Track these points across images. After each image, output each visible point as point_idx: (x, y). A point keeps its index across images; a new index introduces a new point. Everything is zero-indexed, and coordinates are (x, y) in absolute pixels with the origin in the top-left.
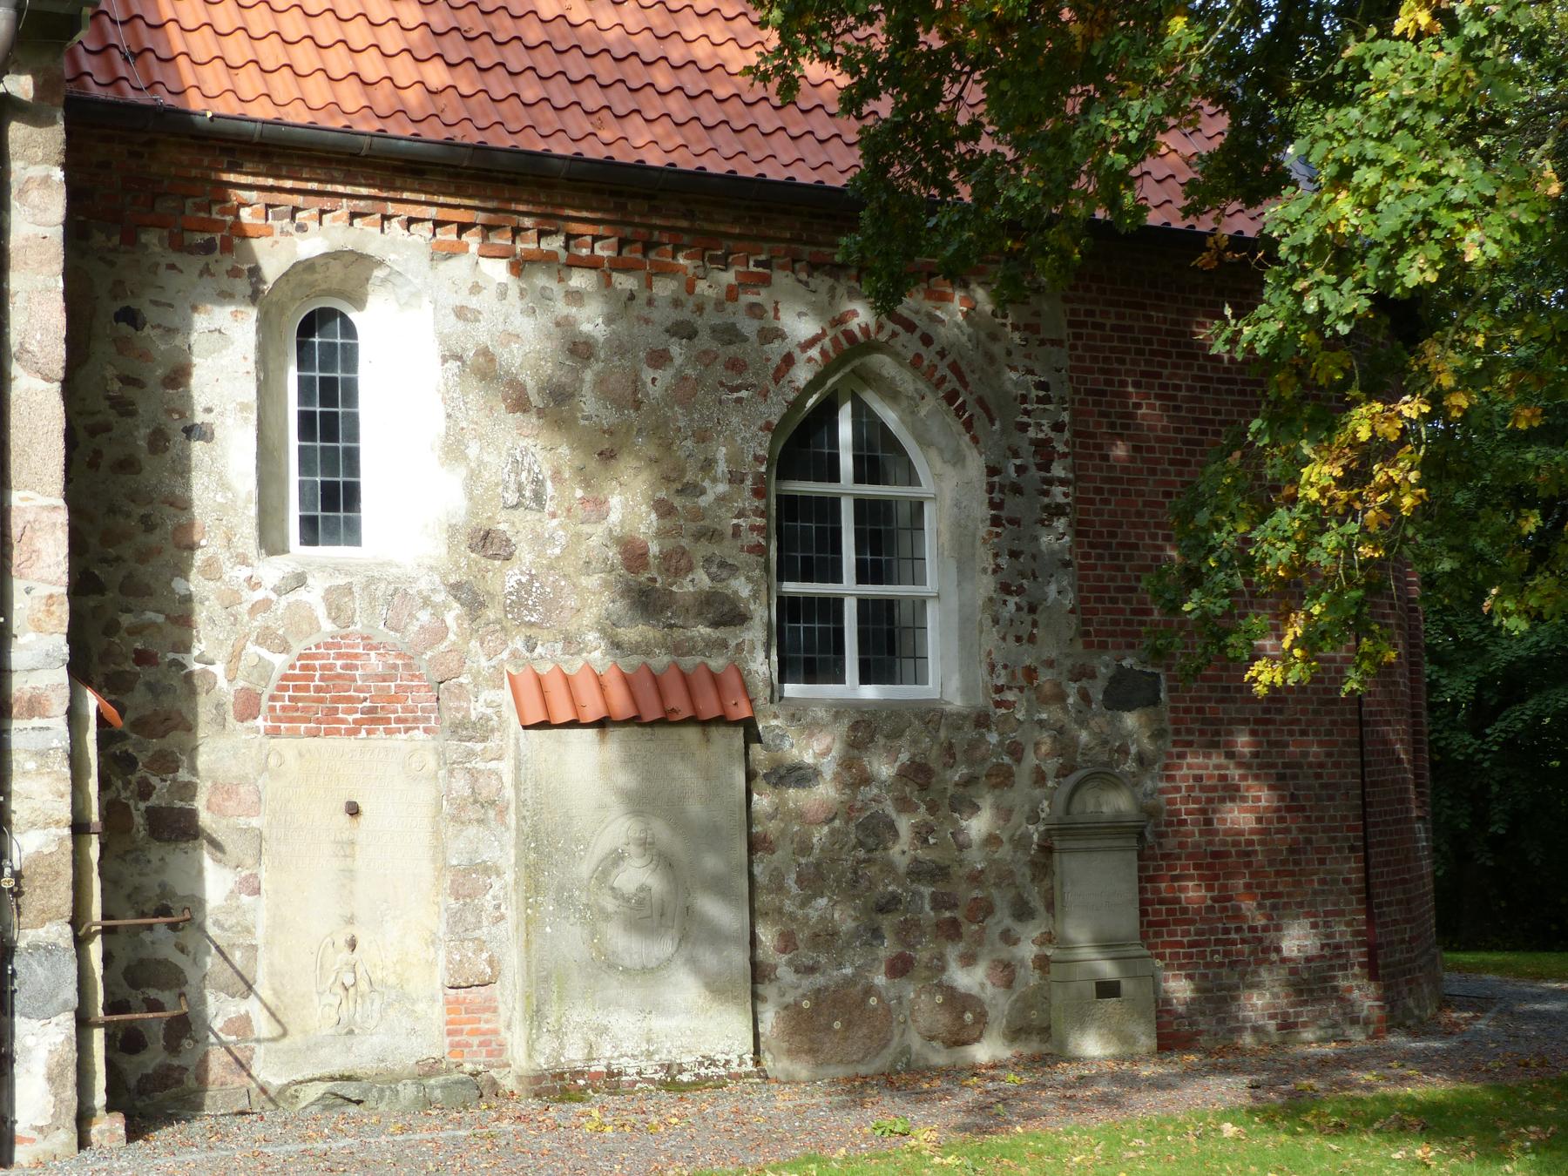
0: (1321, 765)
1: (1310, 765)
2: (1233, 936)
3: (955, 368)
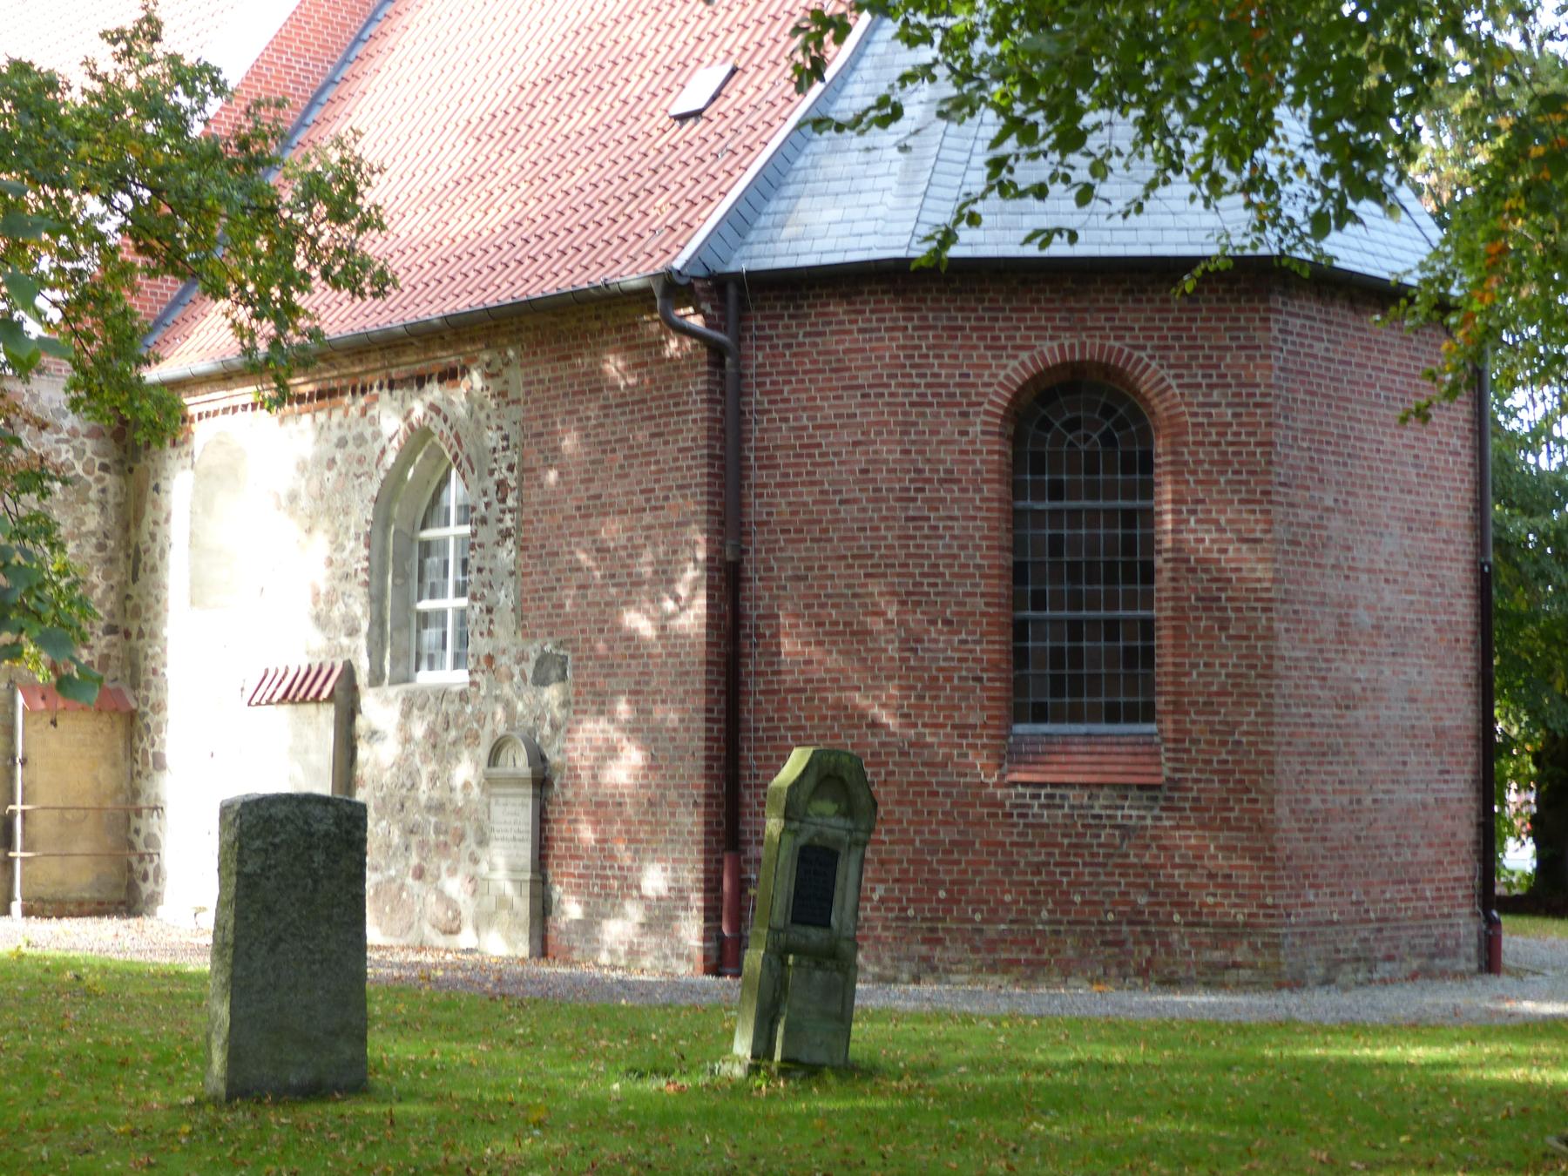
0: (675, 730)
1: (667, 730)
2: (609, 873)
3: (457, 437)
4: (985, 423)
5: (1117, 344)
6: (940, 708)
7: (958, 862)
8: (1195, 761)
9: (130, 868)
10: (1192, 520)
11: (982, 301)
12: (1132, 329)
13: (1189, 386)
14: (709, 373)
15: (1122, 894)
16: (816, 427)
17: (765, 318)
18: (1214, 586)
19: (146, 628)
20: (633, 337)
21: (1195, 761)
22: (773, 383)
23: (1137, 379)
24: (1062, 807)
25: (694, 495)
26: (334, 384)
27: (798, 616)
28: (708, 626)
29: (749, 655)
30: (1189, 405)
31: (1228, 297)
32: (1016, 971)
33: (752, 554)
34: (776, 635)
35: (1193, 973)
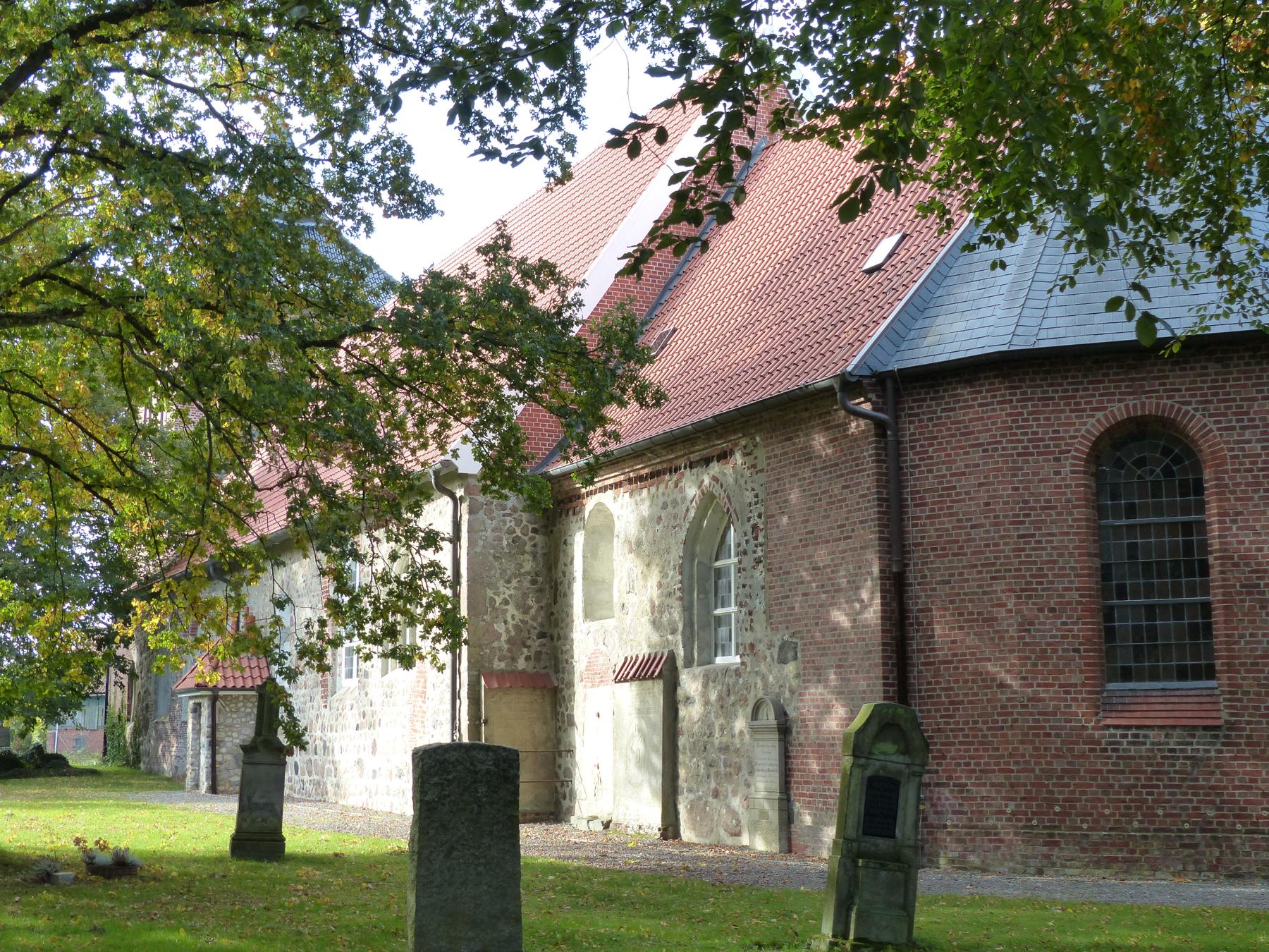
0: (864, 692)
4: (1073, 465)
5: (1169, 402)
6: (1050, 672)
7: (1068, 785)
8: (1246, 708)
9: (556, 791)
10: (1234, 527)
11: (1067, 378)
12: (1180, 390)
13: (1226, 429)
14: (876, 442)
15: (1195, 808)
16: (953, 475)
17: (914, 401)
18: (1254, 576)
19: (561, 633)
20: (829, 422)
21: (1246, 708)
22: (922, 446)
23: (1186, 426)
24: (1144, 744)
25: (870, 527)
26: (659, 467)
27: (946, 609)
28: (882, 618)
29: (912, 638)
30: (1227, 442)
31: (1253, 361)
32: (1115, 866)
33: (912, 567)
34: (930, 623)
35: (1254, 869)
